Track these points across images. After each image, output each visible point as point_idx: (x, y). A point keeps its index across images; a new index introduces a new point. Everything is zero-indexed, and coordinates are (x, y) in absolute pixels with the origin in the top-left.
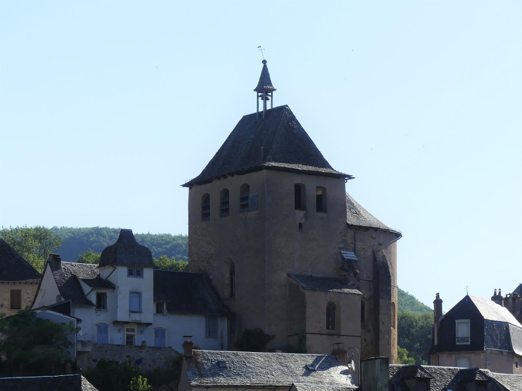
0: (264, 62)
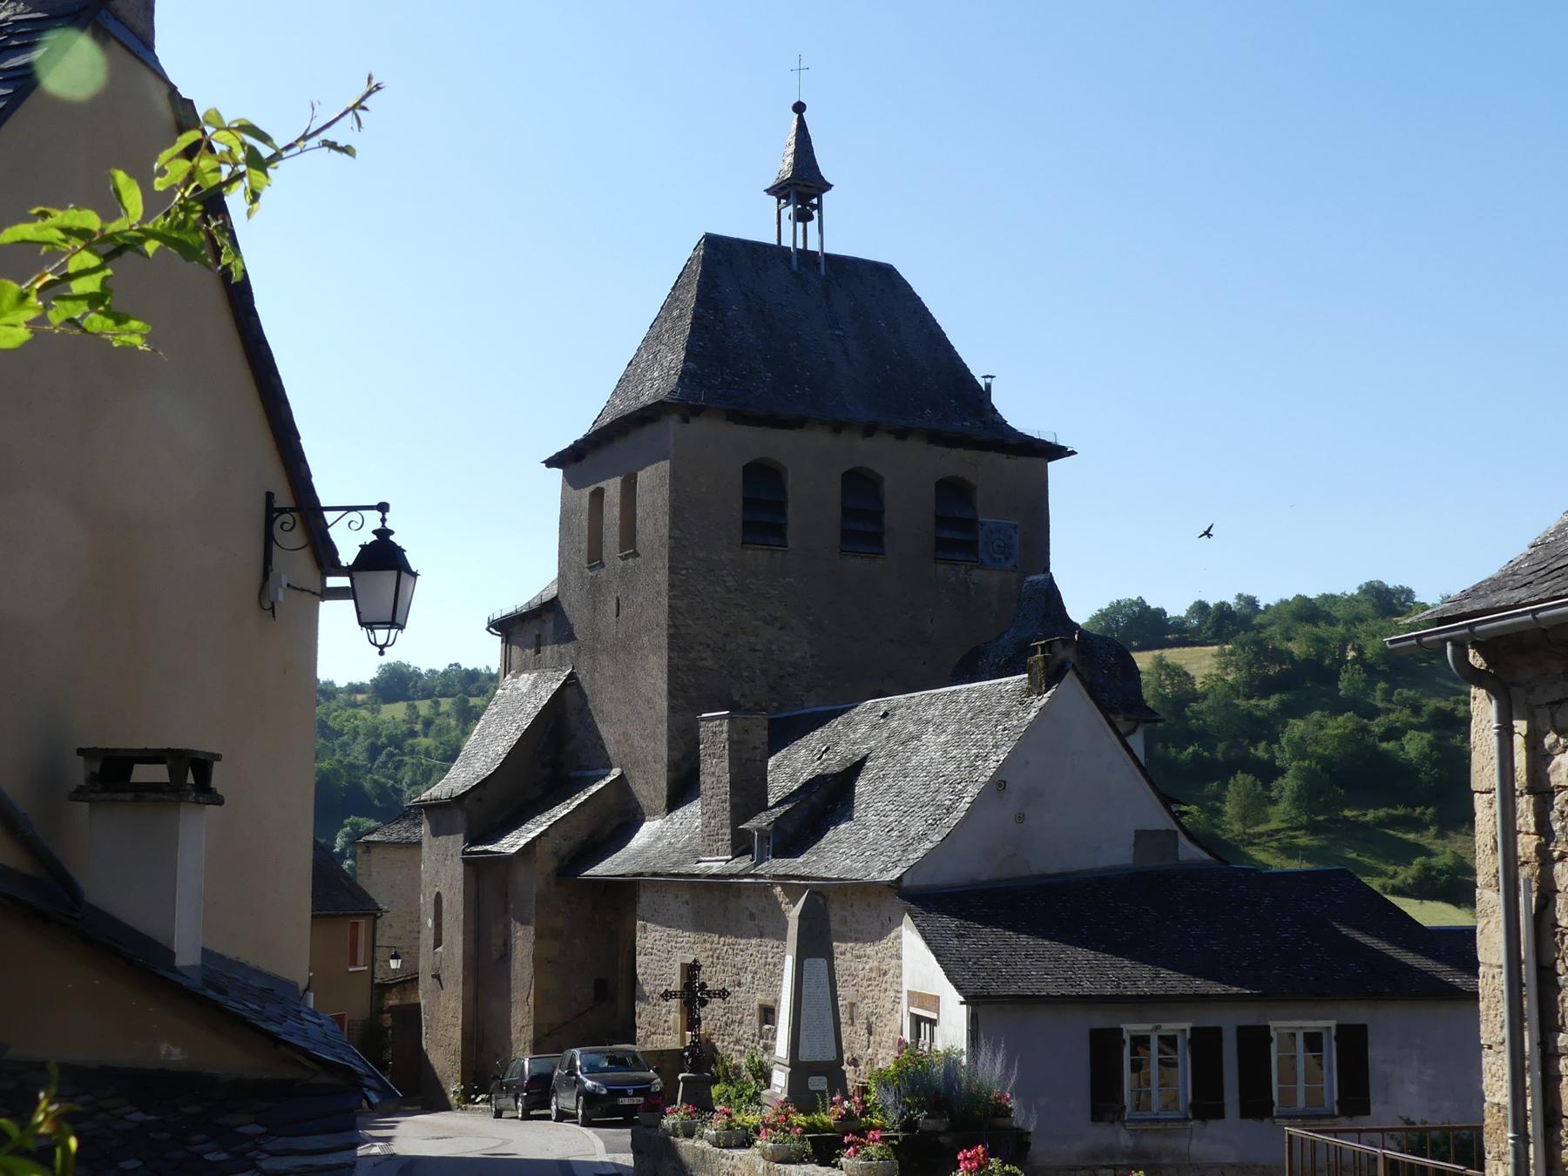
0: (799, 108)
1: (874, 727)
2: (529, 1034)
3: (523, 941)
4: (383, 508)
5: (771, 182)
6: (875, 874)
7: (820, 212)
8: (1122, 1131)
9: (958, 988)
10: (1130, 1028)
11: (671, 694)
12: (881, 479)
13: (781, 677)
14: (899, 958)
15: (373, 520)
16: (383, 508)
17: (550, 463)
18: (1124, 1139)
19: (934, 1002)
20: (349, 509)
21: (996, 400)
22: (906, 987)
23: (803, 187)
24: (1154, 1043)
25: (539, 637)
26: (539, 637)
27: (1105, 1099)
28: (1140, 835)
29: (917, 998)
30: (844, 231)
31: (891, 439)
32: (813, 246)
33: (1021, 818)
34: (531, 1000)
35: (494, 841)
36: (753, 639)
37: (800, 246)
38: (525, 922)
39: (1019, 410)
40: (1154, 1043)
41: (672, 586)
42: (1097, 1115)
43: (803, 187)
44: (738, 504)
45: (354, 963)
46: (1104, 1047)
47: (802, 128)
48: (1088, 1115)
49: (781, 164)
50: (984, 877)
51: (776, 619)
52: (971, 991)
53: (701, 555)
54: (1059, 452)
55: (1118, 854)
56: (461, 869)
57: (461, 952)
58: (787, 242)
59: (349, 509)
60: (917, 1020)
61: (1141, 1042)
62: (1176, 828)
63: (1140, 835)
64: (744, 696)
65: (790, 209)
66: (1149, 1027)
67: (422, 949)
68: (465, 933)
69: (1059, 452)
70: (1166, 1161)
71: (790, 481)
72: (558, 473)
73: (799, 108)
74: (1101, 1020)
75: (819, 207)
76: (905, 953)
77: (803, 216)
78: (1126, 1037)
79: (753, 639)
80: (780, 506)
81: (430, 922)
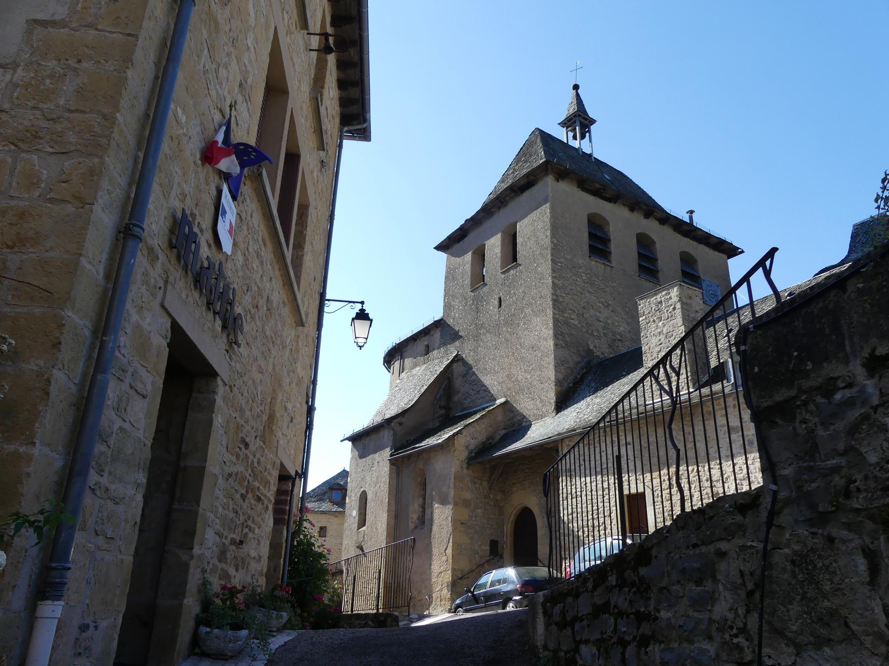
0: (576, 87)
2: (448, 577)
3: (442, 517)
4: (362, 303)
5: (563, 118)
11: (556, 336)
12: (654, 243)
13: (614, 340)
15: (359, 306)
16: (362, 303)
20: (350, 302)
23: (580, 120)
25: (428, 346)
26: (428, 346)
31: (657, 223)
34: (449, 551)
35: (421, 442)
36: (598, 314)
38: (444, 502)
41: (553, 271)
44: (586, 235)
47: (578, 95)
51: (609, 305)
53: (569, 257)
57: (385, 526)
59: (350, 302)
64: (595, 347)
67: (346, 533)
68: (389, 511)
72: (443, 256)
73: (576, 87)
75: (589, 131)
79: (598, 314)
81: (355, 513)
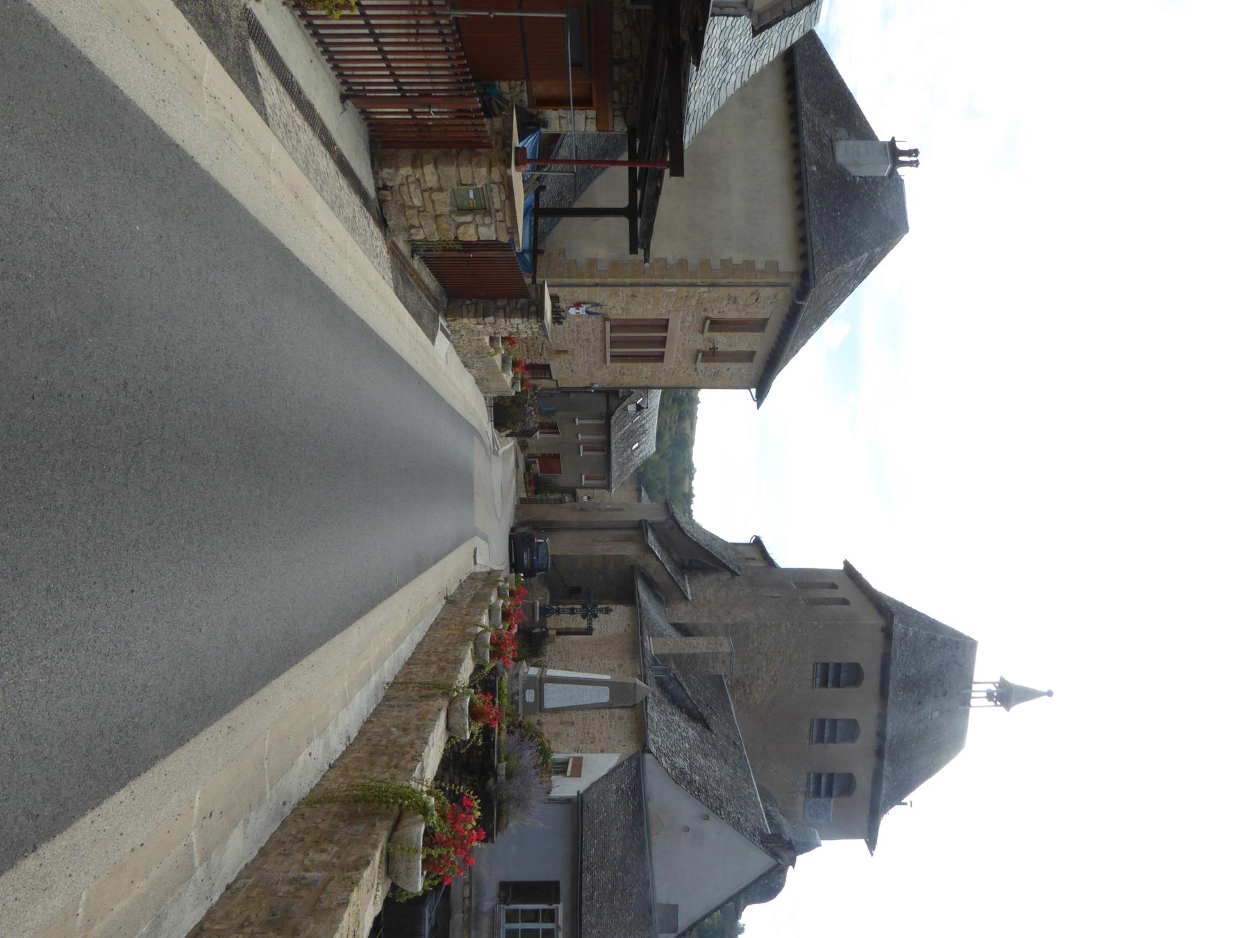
0: (1050, 694)
1: (728, 737)
6: (652, 736)
7: (671, 776)
8: (493, 903)
9: (588, 790)
10: (560, 909)
14: (602, 751)
17: (846, 563)
18: (488, 905)
19: (577, 773)
21: (896, 807)
22: (585, 756)
23: (1006, 695)
24: (549, 926)
27: (513, 891)
28: (675, 908)
29: (578, 763)
30: (982, 717)
32: (973, 702)
33: (687, 829)
37: (973, 694)
39: (892, 821)
40: (549, 926)
42: (504, 886)
43: (1006, 695)
45: (584, 450)
46: (546, 891)
48: (504, 879)
49: (1015, 680)
50: (650, 806)
52: (586, 799)
54: (872, 844)
55: (663, 894)
56: (759, 317)
58: (974, 687)
60: (565, 763)
61: (550, 916)
62: (680, 931)
63: (675, 908)
65: (993, 688)
66: (560, 922)
69: (872, 844)
70: (473, 933)
71: (853, 690)
72: (841, 567)
73: (1050, 694)
74: (564, 890)
76: (606, 756)
77: (990, 696)
78: (554, 906)
80: (837, 684)
